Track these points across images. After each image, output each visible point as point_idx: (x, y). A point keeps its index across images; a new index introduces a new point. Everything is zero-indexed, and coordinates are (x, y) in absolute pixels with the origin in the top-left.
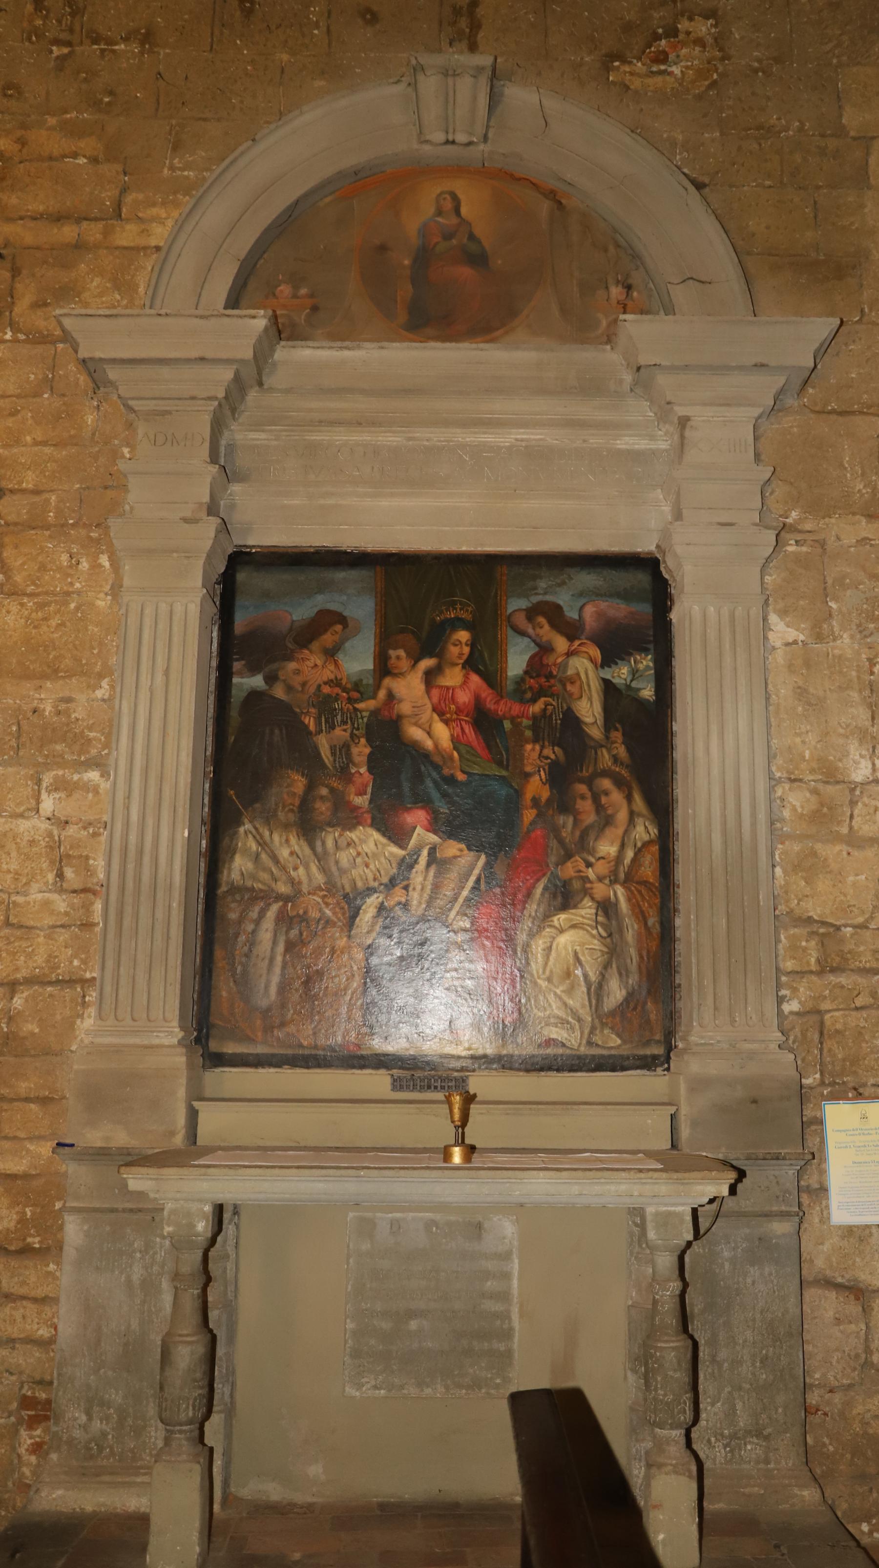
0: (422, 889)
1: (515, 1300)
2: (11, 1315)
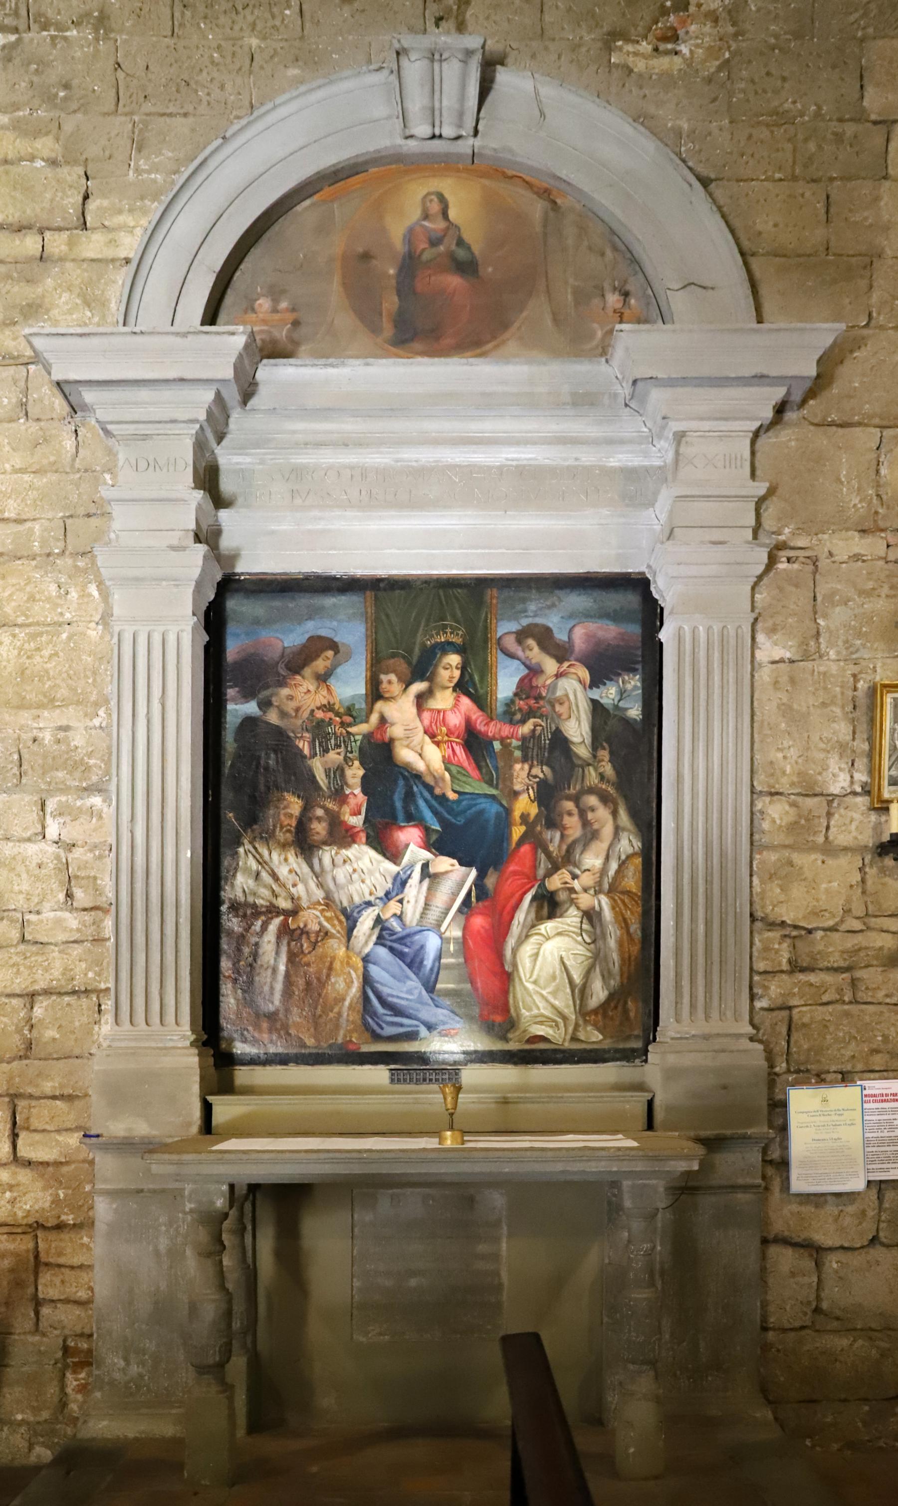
0: (416, 901)
1: (504, 1260)
2: (51, 1281)
